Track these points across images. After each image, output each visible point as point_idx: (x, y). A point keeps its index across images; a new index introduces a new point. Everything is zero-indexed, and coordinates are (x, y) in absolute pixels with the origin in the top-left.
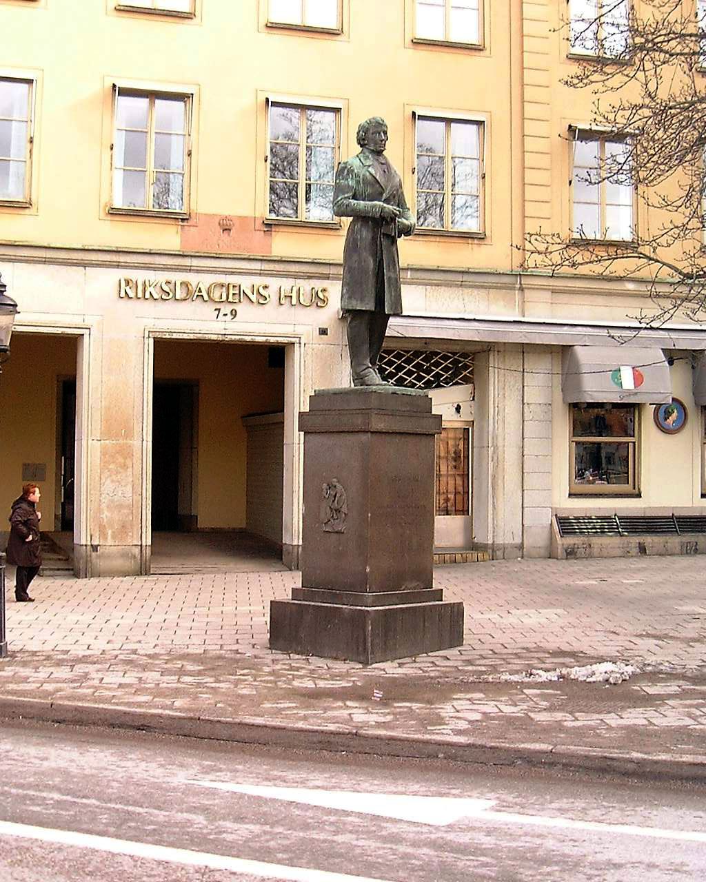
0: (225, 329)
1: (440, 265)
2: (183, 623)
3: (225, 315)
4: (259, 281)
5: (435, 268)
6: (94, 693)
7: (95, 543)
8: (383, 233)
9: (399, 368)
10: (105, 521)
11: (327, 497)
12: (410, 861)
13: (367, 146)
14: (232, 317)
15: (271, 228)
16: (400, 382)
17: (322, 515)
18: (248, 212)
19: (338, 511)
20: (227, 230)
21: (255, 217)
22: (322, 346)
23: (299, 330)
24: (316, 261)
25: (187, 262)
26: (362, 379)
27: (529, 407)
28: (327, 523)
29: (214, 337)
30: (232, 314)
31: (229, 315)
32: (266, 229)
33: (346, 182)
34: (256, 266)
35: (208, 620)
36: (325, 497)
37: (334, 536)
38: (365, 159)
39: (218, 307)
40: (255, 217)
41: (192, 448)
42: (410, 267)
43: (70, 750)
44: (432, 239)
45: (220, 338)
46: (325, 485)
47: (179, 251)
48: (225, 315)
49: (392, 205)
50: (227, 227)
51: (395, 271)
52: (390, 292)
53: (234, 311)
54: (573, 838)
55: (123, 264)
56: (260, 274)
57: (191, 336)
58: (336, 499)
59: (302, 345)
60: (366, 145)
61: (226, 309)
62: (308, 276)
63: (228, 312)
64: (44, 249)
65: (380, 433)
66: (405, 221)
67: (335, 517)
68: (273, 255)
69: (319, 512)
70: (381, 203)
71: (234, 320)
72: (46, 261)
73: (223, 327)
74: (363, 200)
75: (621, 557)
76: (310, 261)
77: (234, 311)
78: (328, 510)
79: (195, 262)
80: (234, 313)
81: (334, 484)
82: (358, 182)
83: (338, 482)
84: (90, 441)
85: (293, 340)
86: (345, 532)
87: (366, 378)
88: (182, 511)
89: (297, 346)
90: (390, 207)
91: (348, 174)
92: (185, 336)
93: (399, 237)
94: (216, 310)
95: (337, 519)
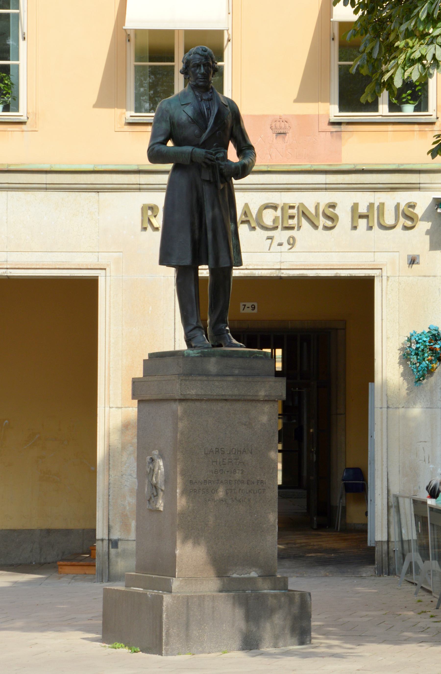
0: (281, 262)
2: (229, 648)
3: (280, 244)
6: (162, 490)
7: (115, 536)
10: (128, 508)
12: (229, 126)
20: (281, 134)
21: (383, 104)
22: (411, 278)
30: (289, 244)
31: (285, 244)
40: (383, 104)
43: (226, 120)
48: (280, 244)
54: (412, 392)
59: (384, 278)
63: (284, 241)
71: (290, 251)
72: (46, 188)
73: (279, 260)
77: (291, 239)
80: (292, 242)
84: (107, 409)
94: (268, 238)
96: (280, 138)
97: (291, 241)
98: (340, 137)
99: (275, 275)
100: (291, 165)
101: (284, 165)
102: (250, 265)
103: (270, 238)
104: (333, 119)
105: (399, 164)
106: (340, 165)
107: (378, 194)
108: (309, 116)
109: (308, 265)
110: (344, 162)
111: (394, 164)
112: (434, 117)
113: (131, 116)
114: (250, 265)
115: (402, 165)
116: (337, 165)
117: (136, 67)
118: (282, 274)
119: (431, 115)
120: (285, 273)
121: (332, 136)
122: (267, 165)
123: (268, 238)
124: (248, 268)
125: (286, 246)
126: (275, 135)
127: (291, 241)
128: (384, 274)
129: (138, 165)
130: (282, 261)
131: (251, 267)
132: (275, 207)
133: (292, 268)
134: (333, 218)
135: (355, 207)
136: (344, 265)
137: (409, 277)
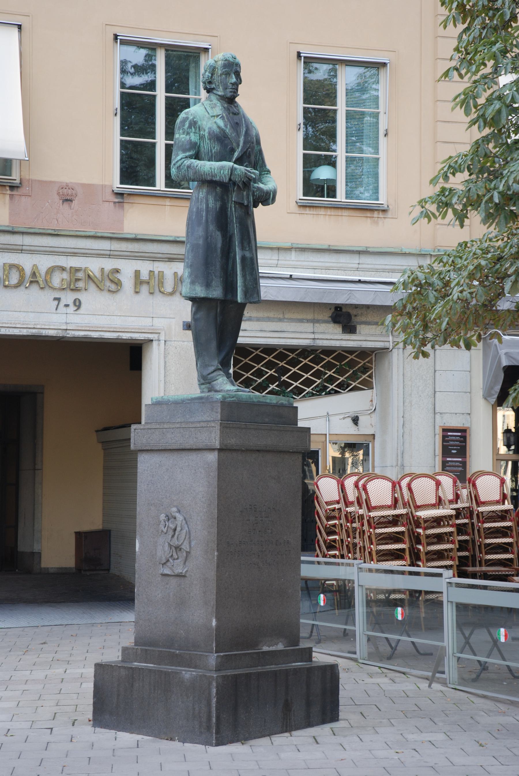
0: (66, 323)
1: (331, 244)
3: (67, 306)
4: (109, 264)
5: (326, 247)
8: (234, 202)
9: (283, 371)
11: (165, 530)
13: (215, 92)
14: (75, 308)
15: (123, 198)
16: (260, 388)
17: (159, 553)
18: (95, 180)
19: (178, 548)
20: (68, 201)
22: (186, 343)
23: (159, 323)
24: (178, 239)
25: (17, 240)
26: (210, 383)
27: (442, 417)
28: (165, 563)
29: (52, 333)
31: (71, 305)
32: (117, 200)
33: (188, 137)
34: (105, 245)
35: (26, 687)
36: (162, 531)
37: (174, 581)
38: (212, 108)
39: (57, 296)
41: (35, 469)
42: (294, 246)
44: (322, 212)
45: (60, 334)
46: (163, 517)
47: (8, 226)
48: (67, 306)
49: (246, 166)
50: (69, 198)
51: (250, 250)
52: (244, 276)
53: (77, 301)
55: (28, 248)
56: (22, 250)
57: (24, 332)
58: (177, 534)
60: (213, 89)
61: (68, 298)
62: (169, 259)
63: (70, 302)
64: (270, 251)
65: (230, 450)
66: (261, 185)
67: (175, 556)
68: (125, 232)
69: (156, 550)
70: (231, 164)
71: (77, 312)
73: (64, 321)
74: (209, 160)
75: (308, 613)
76: (171, 239)
77: (77, 301)
78: (167, 548)
79: (28, 240)
80: (78, 304)
81: (173, 514)
82: (202, 137)
83: (179, 511)
85: (151, 336)
86: (187, 575)
87: (215, 382)
88: (22, 547)
89: (155, 344)
90: (242, 168)
91: (190, 127)
92: (16, 332)
93: (256, 206)
94: (55, 299)
95: (177, 559)
96: (66, 205)
97: (77, 304)
98: (123, 207)
99: (373, 347)
100: (76, 231)
101: (70, 230)
102: (38, 324)
103: (58, 299)
104: (116, 190)
105: (175, 237)
106: (122, 233)
107: (156, 264)
108: (93, 185)
109: (92, 327)
110: (125, 231)
111: (171, 236)
112: (18, 181)
113: (300, 199)
114: (38, 324)
115: (178, 237)
116: (119, 233)
117: (122, 141)
118: (68, 334)
119: (15, 180)
120: (71, 334)
121: (115, 206)
122: (54, 230)
123: (55, 299)
124: (35, 327)
125: (72, 308)
126: (61, 201)
127: (77, 304)
128: (162, 338)
129: (366, 247)
130: (68, 322)
131: (38, 327)
132: (63, 269)
133: (77, 329)
134: (118, 283)
135: (137, 273)
136: (126, 328)
137: (184, 342)
